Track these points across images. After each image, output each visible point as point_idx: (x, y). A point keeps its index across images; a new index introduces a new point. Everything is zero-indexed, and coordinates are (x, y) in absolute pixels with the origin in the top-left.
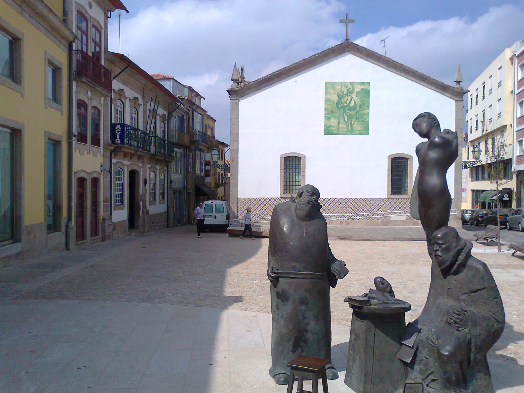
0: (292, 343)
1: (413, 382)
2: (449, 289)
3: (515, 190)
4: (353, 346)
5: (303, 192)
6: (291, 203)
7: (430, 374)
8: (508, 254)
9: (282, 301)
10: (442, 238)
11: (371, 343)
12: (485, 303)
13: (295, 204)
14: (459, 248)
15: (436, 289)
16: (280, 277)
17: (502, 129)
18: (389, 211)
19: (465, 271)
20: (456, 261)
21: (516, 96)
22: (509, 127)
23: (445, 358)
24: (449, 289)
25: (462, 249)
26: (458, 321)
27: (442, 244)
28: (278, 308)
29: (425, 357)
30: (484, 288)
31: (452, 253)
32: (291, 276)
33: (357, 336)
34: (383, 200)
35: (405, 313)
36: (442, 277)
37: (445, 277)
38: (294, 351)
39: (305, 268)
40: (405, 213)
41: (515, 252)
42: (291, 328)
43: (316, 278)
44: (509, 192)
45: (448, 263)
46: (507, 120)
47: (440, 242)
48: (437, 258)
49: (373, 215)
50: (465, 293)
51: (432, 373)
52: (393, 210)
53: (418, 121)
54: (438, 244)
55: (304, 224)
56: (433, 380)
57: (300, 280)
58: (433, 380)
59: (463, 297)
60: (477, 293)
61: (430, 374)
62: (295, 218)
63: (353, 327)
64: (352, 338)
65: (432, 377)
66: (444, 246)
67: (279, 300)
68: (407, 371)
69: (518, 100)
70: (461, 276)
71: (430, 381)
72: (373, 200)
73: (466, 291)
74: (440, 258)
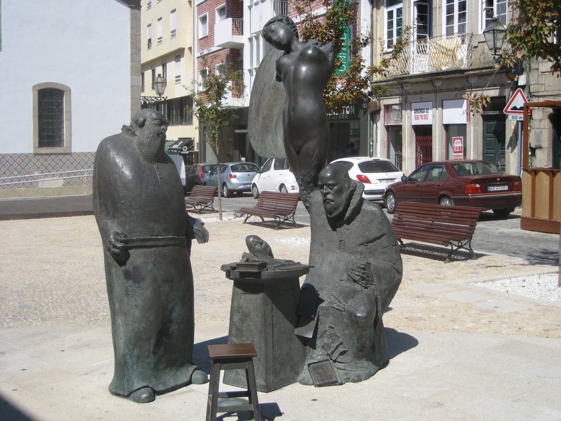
0: (153, 341)
1: (315, 361)
2: (341, 241)
3: (197, 140)
4: (238, 330)
5: (145, 121)
6: (127, 137)
7: (338, 346)
8: (240, 221)
9: (135, 282)
10: (333, 177)
11: (269, 320)
12: (384, 253)
13: (137, 138)
14: (351, 189)
15: (322, 244)
16: (131, 248)
17: (177, 55)
18: (37, 174)
19: (359, 217)
20: (349, 206)
21: (196, 8)
22: (187, 52)
23: (363, 321)
24: (341, 241)
25: (354, 190)
26: (365, 276)
27: (334, 185)
28: (127, 294)
29: (330, 327)
30: (383, 235)
31: (345, 196)
32: (148, 244)
33: (245, 316)
34: (27, 156)
35: (300, 278)
36: (330, 229)
37: (334, 229)
38: (155, 353)
39: (166, 231)
40: (61, 175)
41: (248, 218)
42: (152, 319)
43: (174, 245)
44: (189, 143)
45: (341, 209)
46: (186, 40)
47: (330, 182)
48: (328, 203)
49: (12, 181)
50: (362, 244)
51: (341, 344)
52: (42, 172)
53: (273, 27)
54: (328, 185)
55: (155, 166)
56: (342, 353)
57: (160, 249)
58: (342, 353)
59: (360, 248)
60: (376, 242)
61: (338, 346)
62: (142, 159)
63: (236, 304)
64: (236, 319)
65: (341, 349)
66: (336, 188)
67: (130, 282)
68: (305, 350)
69: (198, 14)
70: (355, 224)
71: (338, 354)
72: (11, 156)
73: (362, 241)
74: (332, 203)
